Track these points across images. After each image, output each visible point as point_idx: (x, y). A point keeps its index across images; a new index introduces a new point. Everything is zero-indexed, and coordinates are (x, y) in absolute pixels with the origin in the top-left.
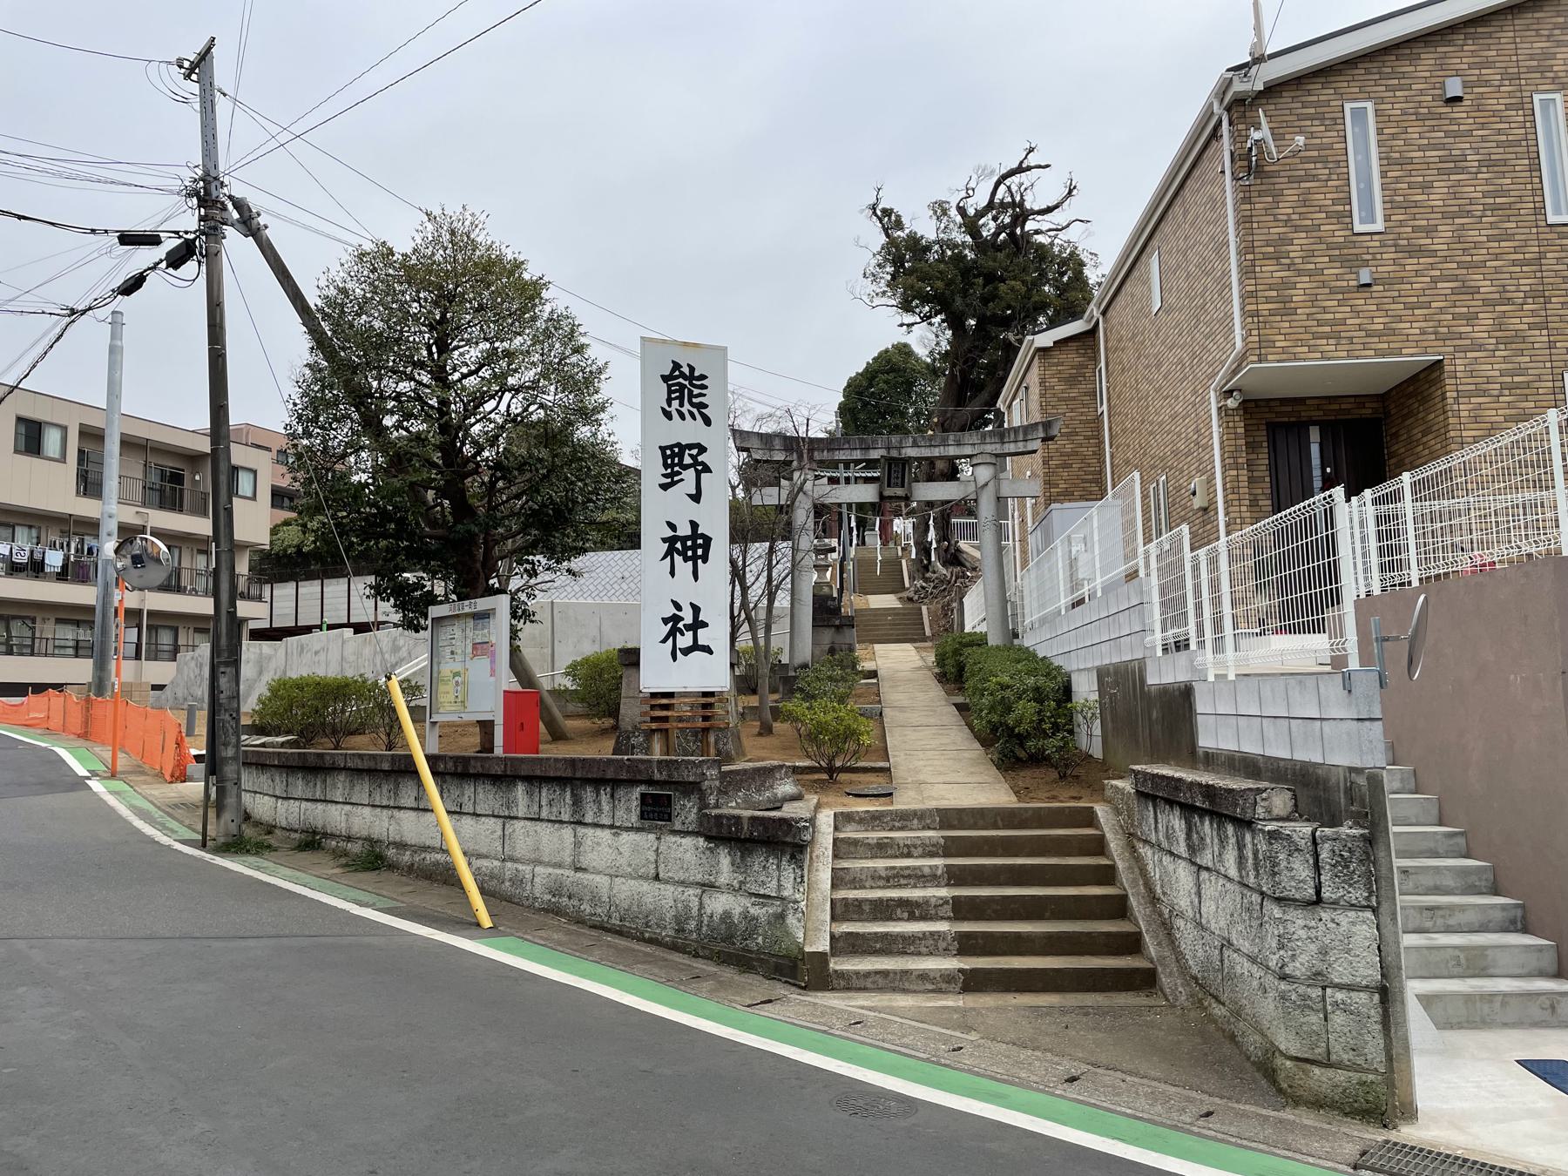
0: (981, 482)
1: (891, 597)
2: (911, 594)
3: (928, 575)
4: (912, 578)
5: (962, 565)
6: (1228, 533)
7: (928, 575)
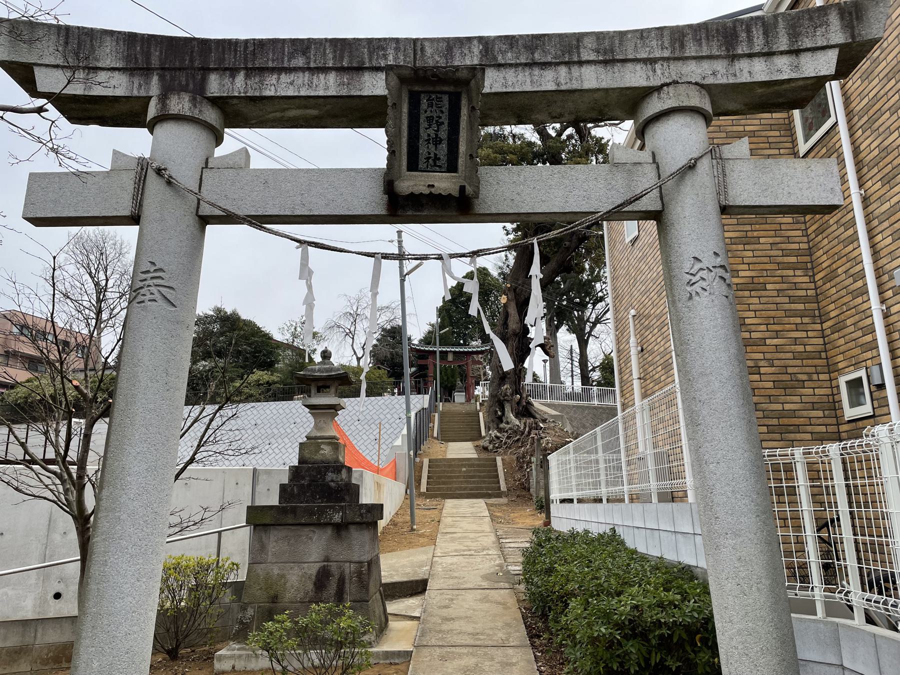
0: (674, 160)
1: (469, 445)
2: (486, 444)
3: (502, 425)
4: (488, 428)
5: (534, 418)
6: (623, 410)
7: (502, 425)
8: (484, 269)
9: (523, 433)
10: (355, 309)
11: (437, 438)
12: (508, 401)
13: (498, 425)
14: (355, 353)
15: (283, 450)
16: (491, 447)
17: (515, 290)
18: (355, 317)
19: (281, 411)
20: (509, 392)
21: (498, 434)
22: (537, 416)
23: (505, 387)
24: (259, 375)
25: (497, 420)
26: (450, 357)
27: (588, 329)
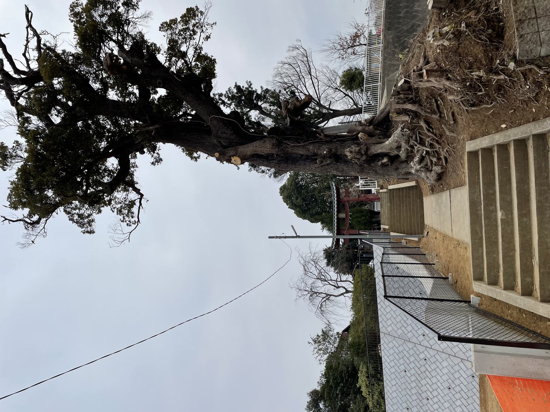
2: (432, 176)
3: (403, 154)
4: (407, 176)
5: (389, 113)
7: (403, 154)
8: (281, 189)
9: (416, 115)
11: (420, 240)
12: (367, 149)
13: (402, 162)
14: (342, 294)
15: (434, 387)
17: (225, 147)
18: (313, 293)
19: (394, 382)
20: (355, 148)
21: (416, 159)
22: (387, 109)
23: (348, 154)
24: (362, 381)
25: (395, 164)
26: (343, 215)
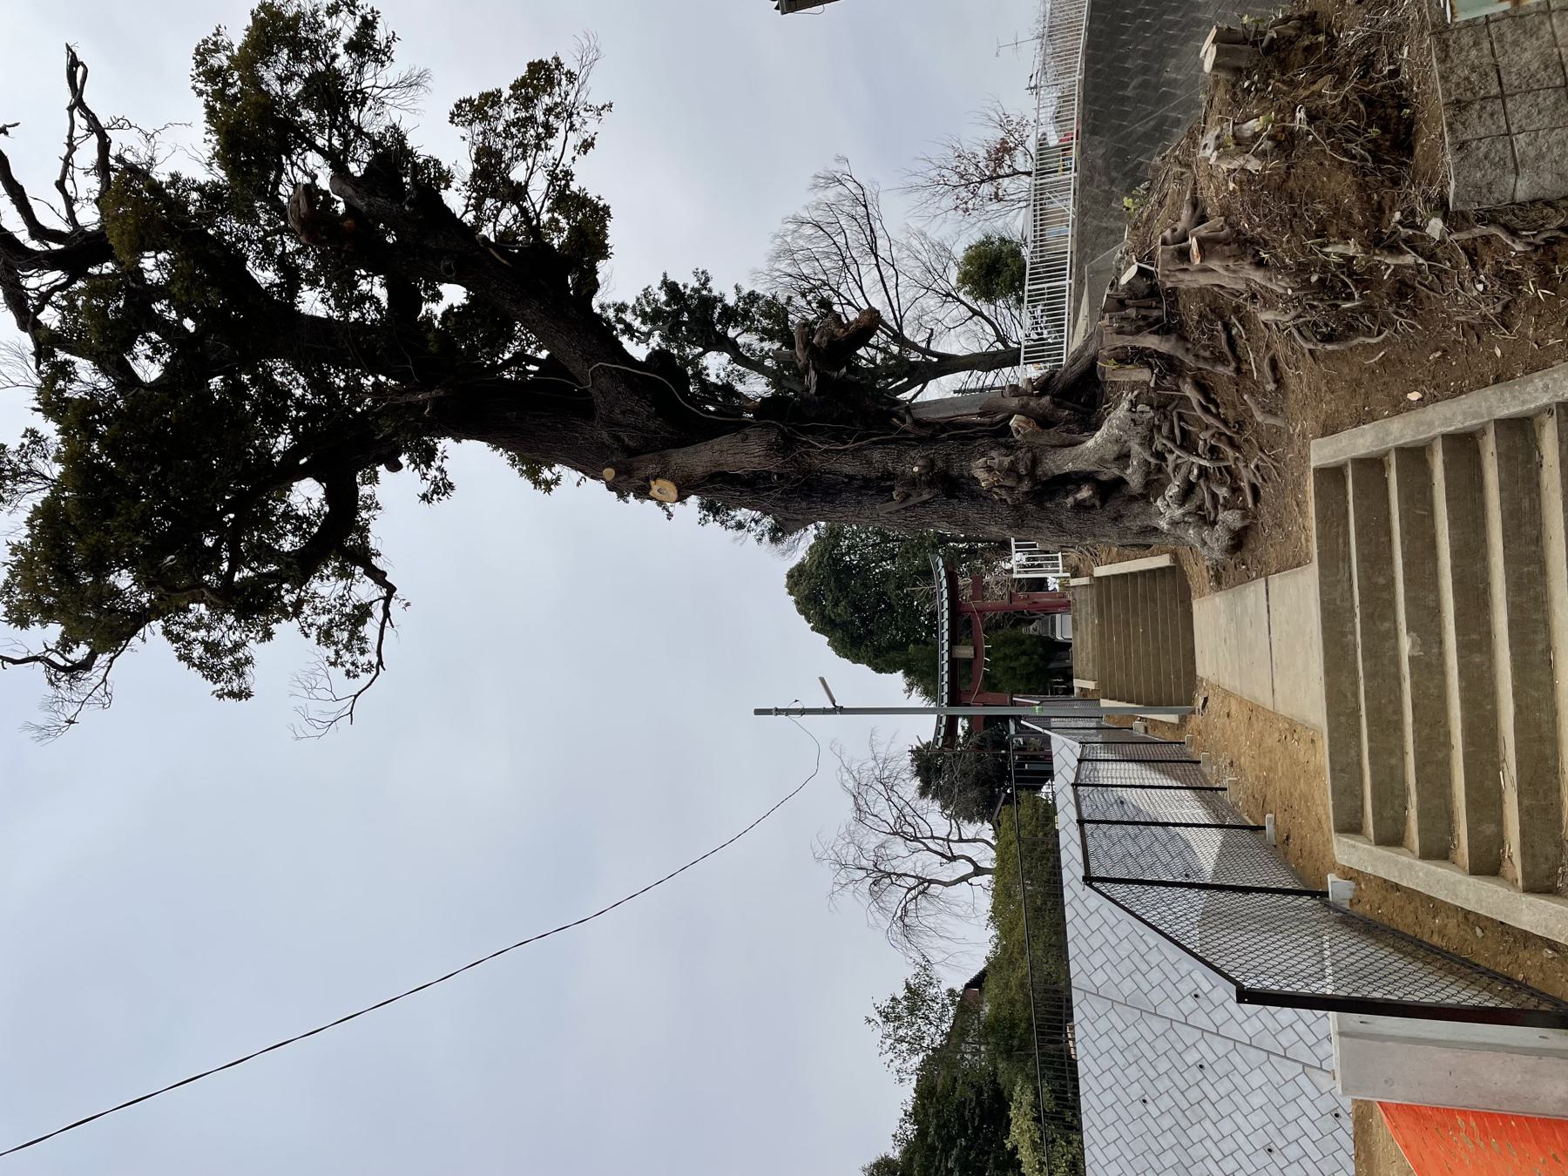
2: (1217, 539)
3: (1134, 477)
4: (1146, 539)
7: (1134, 477)
8: (790, 576)
9: (1170, 366)
10: (863, 874)
12: (1035, 462)
13: (1133, 499)
14: (964, 879)
15: (1228, 1146)
16: (1231, 518)
17: (633, 453)
18: (882, 876)
19: (1111, 1134)
20: (999, 458)
21: (1173, 490)
22: (1091, 351)
23: (980, 474)
26: (966, 652)
27: (914, 357)
